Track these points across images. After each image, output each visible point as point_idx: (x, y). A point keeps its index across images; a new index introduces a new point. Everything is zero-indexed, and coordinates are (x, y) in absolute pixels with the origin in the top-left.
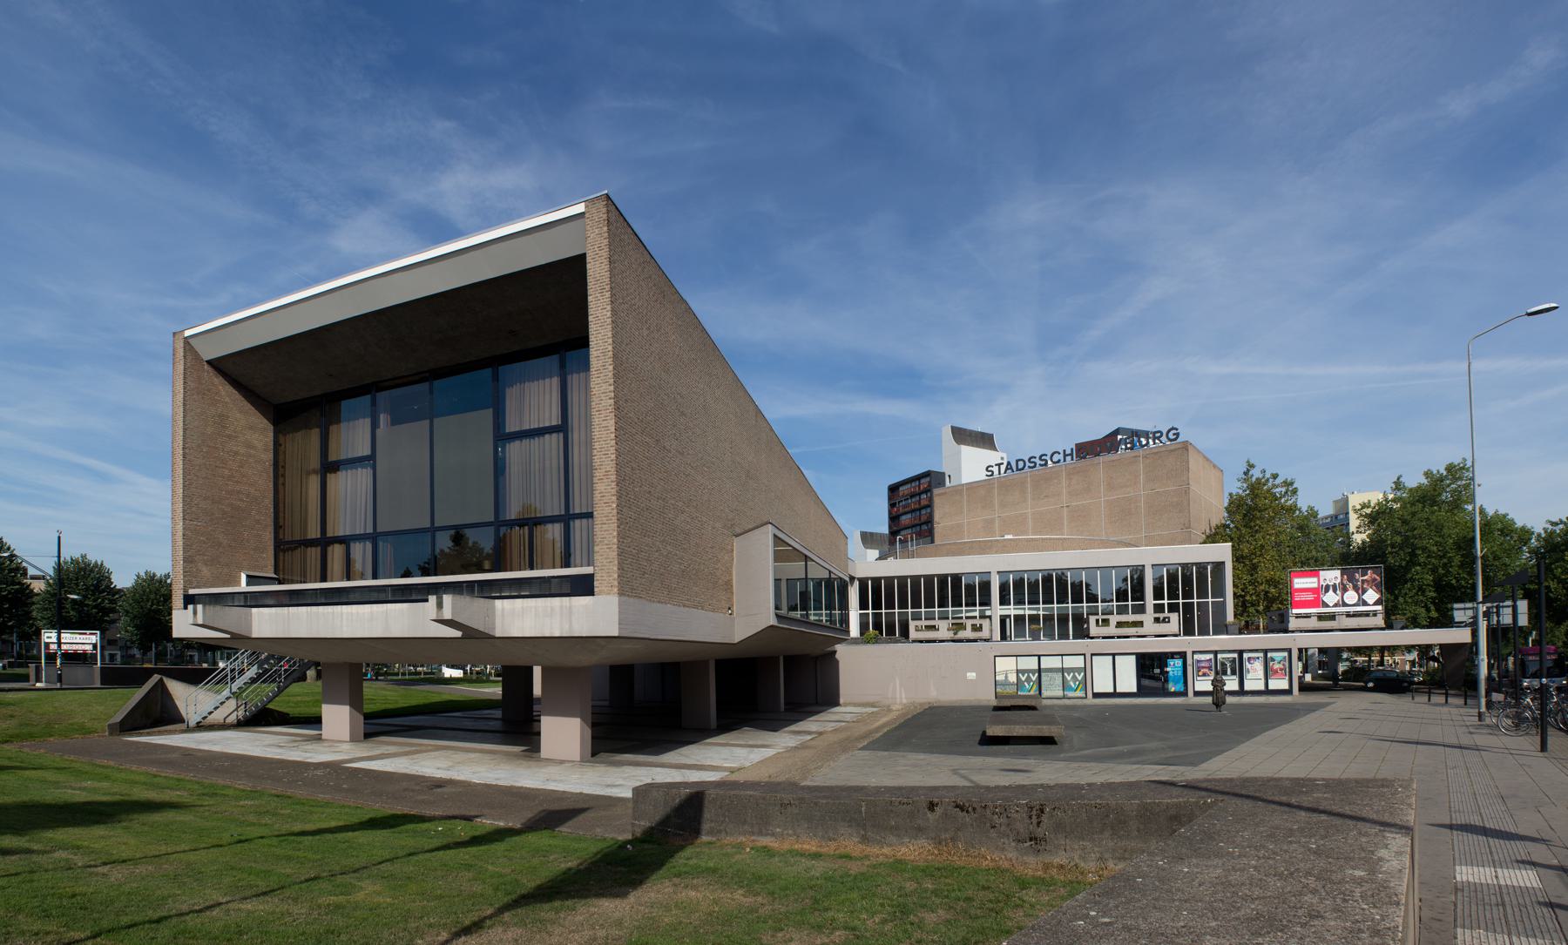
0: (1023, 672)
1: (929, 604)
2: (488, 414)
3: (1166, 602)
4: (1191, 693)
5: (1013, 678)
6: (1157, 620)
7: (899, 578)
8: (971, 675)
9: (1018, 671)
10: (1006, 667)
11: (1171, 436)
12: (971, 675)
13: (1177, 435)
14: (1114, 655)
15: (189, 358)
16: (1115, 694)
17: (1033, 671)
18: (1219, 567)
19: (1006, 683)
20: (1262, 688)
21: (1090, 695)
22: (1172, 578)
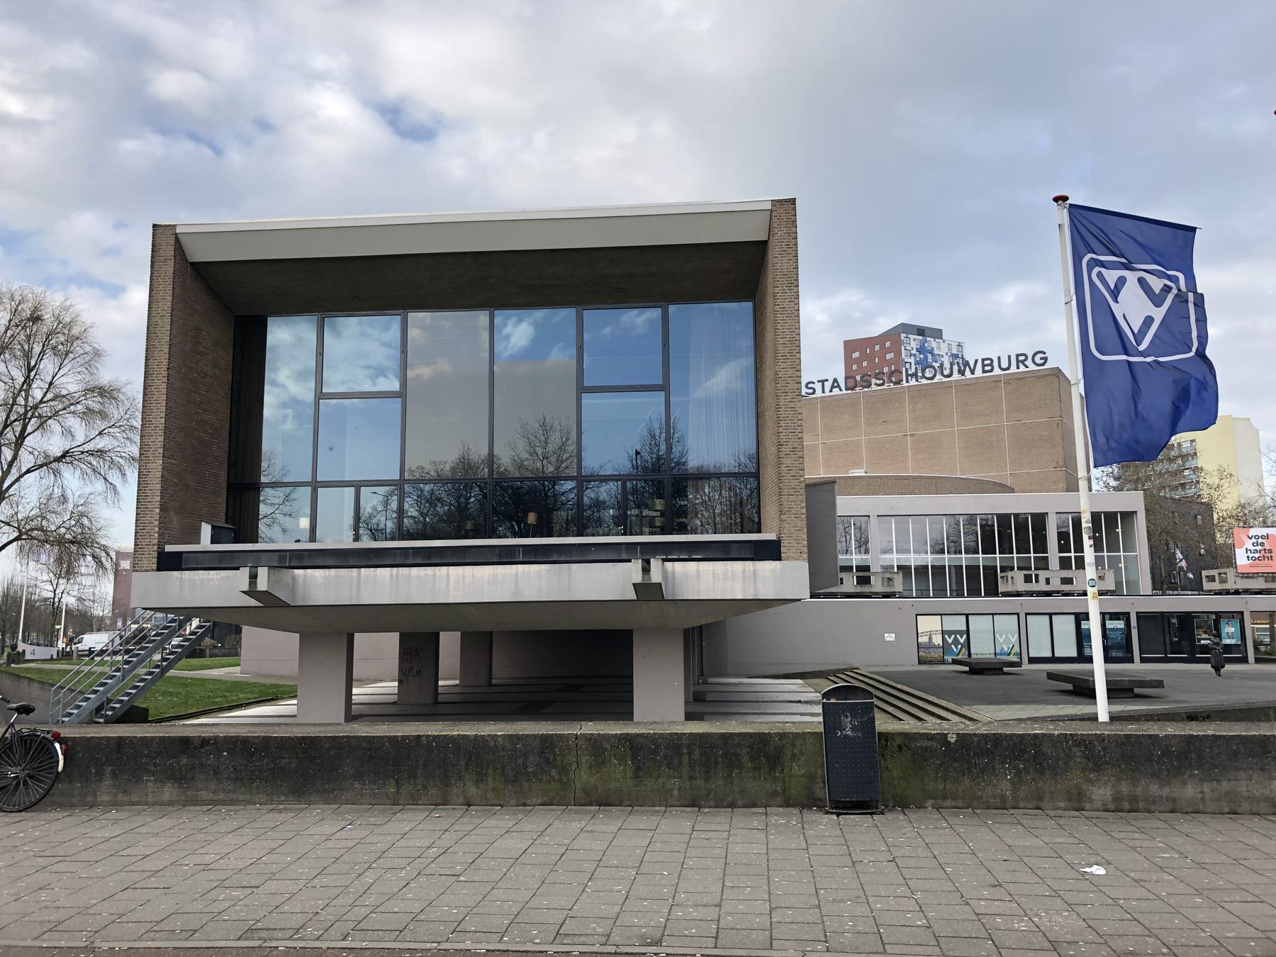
0: (950, 633)
1: (1006, 549)
2: (748, 305)
3: (1015, 555)
4: (1025, 659)
5: (937, 640)
6: (1037, 581)
7: (1016, 515)
8: (890, 637)
9: (943, 633)
10: (930, 627)
11: (1038, 360)
12: (890, 637)
13: (1046, 359)
14: (1050, 615)
15: (178, 258)
16: (1053, 660)
17: (961, 633)
18: (1128, 516)
19: (930, 646)
20: (1049, 654)
21: (1025, 659)
22: (987, 529)
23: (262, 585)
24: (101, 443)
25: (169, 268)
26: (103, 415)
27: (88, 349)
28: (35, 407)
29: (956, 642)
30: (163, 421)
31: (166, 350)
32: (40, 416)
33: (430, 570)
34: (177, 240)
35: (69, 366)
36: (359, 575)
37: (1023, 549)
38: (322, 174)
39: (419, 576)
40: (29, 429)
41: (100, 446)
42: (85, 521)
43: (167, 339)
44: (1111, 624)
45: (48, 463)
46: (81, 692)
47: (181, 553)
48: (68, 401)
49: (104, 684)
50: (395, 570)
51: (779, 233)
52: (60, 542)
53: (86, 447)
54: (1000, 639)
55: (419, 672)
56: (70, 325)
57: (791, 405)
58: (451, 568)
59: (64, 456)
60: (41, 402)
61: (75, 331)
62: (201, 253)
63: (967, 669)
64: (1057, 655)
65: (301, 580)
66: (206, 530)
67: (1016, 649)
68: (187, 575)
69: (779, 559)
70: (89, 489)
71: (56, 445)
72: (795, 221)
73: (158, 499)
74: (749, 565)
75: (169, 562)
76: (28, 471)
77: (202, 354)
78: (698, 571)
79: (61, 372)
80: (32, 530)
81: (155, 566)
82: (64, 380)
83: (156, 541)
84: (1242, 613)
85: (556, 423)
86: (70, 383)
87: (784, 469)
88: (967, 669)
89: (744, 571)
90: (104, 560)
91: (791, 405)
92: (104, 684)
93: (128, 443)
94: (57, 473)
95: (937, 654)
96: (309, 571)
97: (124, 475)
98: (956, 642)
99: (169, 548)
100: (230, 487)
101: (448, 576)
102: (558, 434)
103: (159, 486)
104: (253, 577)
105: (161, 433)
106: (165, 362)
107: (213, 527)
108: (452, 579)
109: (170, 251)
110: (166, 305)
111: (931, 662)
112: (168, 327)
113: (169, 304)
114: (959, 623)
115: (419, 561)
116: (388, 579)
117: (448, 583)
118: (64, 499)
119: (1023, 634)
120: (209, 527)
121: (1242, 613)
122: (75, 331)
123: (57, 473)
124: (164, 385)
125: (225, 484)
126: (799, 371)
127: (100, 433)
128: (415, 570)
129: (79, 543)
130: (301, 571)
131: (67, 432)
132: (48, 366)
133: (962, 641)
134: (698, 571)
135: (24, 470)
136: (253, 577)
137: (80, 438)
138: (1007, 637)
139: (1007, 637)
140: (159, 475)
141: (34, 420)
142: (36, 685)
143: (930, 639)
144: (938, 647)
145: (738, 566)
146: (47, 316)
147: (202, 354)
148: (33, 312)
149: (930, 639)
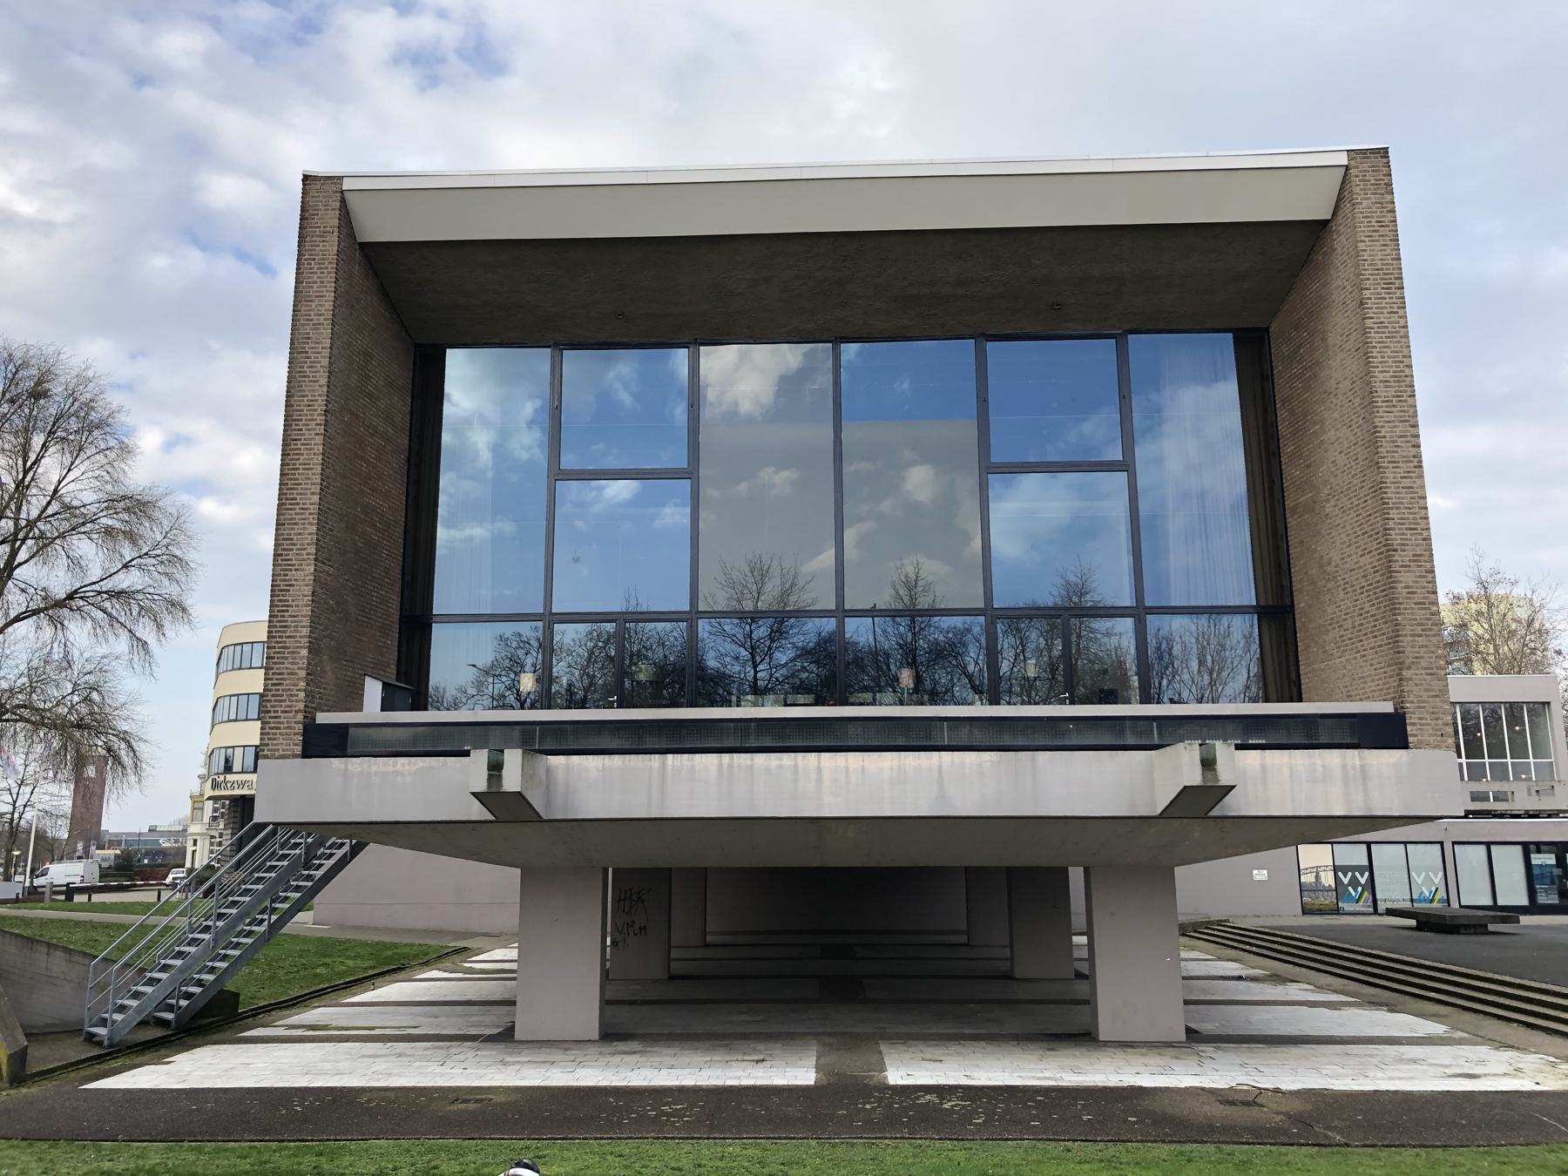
5: (1328, 879)
9: (1336, 869)
14: (1488, 845)
17: (1361, 869)
19: (1317, 887)
23: (512, 780)
24: (125, 581)
25: (331, 246)
26: (132, 537)
27: (112, 443)
28: (31, 524)
29: (1354, 883)
30: (316, 498)
31: (324, 381)
32: (42, 535)
33: (787, 759)
34: (343, 201)
35: (82, 467)
36: (664, 765)
37: (1497, 751)
38: (548, 139)
39: (780, 767)
40: (22, 555)
41: (124, 586)
42: (95, 695)
43: (325, 362)
44: (1536, 859)
45: (53, 608)
46: (142, 970)
47: (346, 726)
48: (76, 520)
49: (180, 955)
50: (726, 757)
51: (1365, 202)
52: (59, 725)
53: (106, 585)
54: (1418, 879)
55: (643, 929)
56: (89, 406)
57: (1406, 483)
58: (825, 756)
59: (70, 597)
60: (39, 518)
61: (93, 416)
62: (379, 228)
63: (1413, 923)
64: (1500, 903)
65: (560, 777)
66: (373, 691)
67: (1442, 894)
68: (356, 765)
69: (1406, 747)
70: (102, 650)
71: (59, 581)
72: (1390, 184)
73: (306, 631)
74: (1353, 756)
75: (324, 743)
76: (17, 619)
77: (370, 395)
78: (1263, 767)
79: (71, 476)
80: (19, 706)
81: (298, 749)
82: (72, 487)
83: (301, 706)
84: (1441, 843)
85: (775, 564)
86: (83, 489)
87: (1401, 590)
88: (1413, 923)
89: (1344, 767)
90: (123, 753)
91: (1406, 483)
92: (180, 955)
93: (166, 581)
94: (57, 623)
95: (1328, 900)
96: (575, 759)
97: (160, 627)
98: (1354, 883)
99: (323, 718)
100: (403, 619)
101: (819, 769)
102: (777, 581)
103: (307, 611)
104: (495, 768)
105: (313, 519)
106: (321, 400)
107: (385, 684)
108: (826, 774)
109: (333, 220)
110: (324, 306)
111: (1320, 912)
112: (327, 343)
113: (329, 305)
114: (1357, 855)
115: (768, 743)
116: (713, 772)
117: (819, 780)
118: (68, 662)
119: (1448, 867)
120: (379, 685)
121: (1441, 843)
122: (93, 416)
123: (57, 623)
124: (320, 439)
125: (396, 617)
126: (1415, 426)
127: (126, 566)
128: (760, 759)
129: (88, 727)
130: (561, 759)
131: (75, 564)
132: (51, 468)
133: (1363, 881)
134: (1263, 767)
135: (13, 614)
136: (495, 768)
137: (95, 573)
138: (1354, 877)
139: (1354, 877)
140: (308, 590)
141: (30, 542)
142: (59, 954)
143: (1317, 877)
144: (1329, 890)
145: (1333, 757)
146: (57, 389)
147: (370, 395)
148: (39, 383)
149: (1317, 877)
